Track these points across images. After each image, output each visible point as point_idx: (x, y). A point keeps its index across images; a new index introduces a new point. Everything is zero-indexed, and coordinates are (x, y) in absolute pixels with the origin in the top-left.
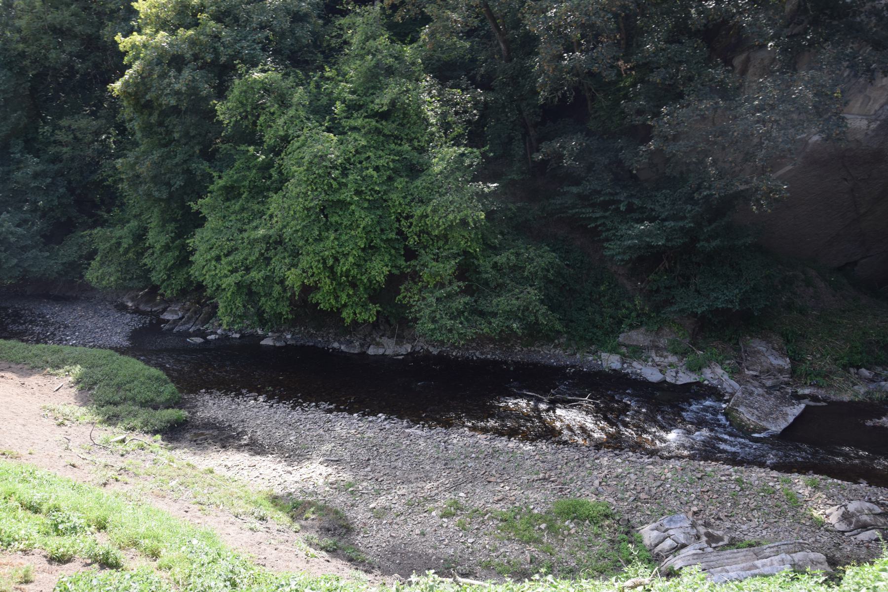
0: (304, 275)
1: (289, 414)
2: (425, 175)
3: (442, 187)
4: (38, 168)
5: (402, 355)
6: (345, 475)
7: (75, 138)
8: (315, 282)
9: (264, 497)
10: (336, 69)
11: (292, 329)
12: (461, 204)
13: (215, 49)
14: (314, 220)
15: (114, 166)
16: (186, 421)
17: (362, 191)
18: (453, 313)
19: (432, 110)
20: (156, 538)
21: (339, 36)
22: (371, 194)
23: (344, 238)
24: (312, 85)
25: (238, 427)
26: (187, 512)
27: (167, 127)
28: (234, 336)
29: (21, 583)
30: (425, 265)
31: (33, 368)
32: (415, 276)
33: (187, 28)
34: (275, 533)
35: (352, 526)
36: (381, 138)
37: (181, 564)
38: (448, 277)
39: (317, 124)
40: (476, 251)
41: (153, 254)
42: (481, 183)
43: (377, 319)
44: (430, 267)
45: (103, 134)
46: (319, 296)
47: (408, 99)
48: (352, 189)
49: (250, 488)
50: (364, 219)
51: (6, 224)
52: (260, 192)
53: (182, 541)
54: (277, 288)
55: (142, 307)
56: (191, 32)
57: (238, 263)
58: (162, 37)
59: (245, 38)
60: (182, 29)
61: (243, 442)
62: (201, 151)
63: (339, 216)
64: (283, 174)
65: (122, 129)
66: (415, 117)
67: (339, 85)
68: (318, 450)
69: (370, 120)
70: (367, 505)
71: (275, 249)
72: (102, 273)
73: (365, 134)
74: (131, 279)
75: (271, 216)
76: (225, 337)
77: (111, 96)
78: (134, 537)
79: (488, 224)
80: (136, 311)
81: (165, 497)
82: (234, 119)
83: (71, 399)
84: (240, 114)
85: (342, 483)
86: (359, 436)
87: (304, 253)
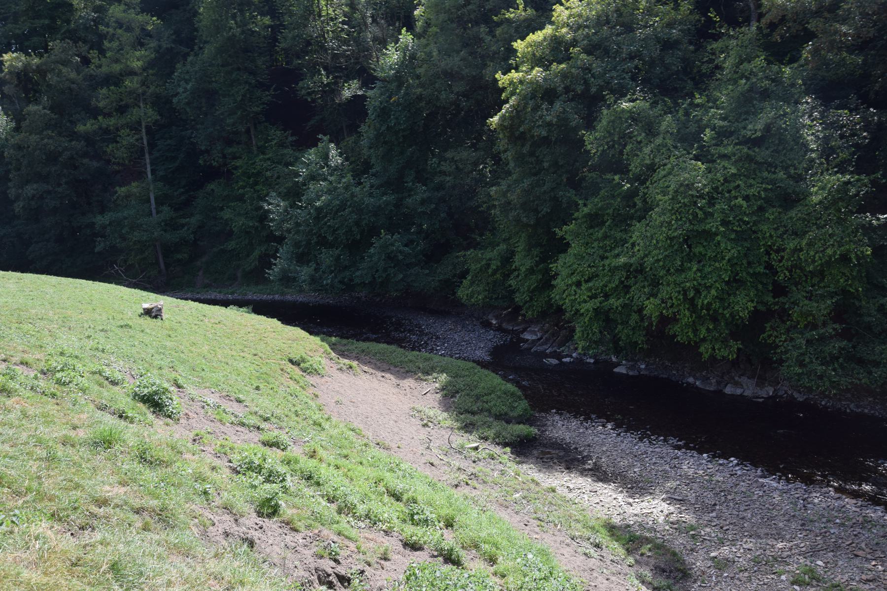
0: (663, 305)
1: (635, 445)
2: (801, 205)
3: (820, 218)
4: (425, 196)
5: (763, 398)
6: (687, 517)
7: (457, 168)
8: (674, 313)
9: (602, 524)
10: (707, 96)
11: (647, 360)
12: (842, 238)
13: (586, 82)
14: (676, 250)
15: (489, 194)
16: (535, 438)
17: (730, 221)
18: (825, 358)
19: (813, 134)
20: (496, 545)
21: (711, 61)
22: (739, 225)
23: (708, 269)
24: (681, 112)
25: (583, 451)
26: (526, 525)
27: (537, 157)
28: (588, 361)
29: (381, 559)
30: (795, 303)
31: (407, 372)
32: (784, 315)
33: (560, 63)
34: (609, 563)
35: (689, 572)
36: (753, 166)
37: (514, 575)
38: (822, 318)
39: (685, 152)
40: (857, 291)
41: (518, 276)
42: (868, 214)
43: (738, 357)
44: (801, 305)
45: (481, 164)
46: (677, 328)
47: (785, 123)
48: (719, 219)
49: (590, 513)
50: (729, 251)
51: (397, 244)
52: (623, 221)
53: (518, 553)
54: (635, 317)
55: (504, 325)
56: (563, 66)
57: (598, 289)
58: (537, 73)
59: (615, 68)
60: (555, 64)
61: (587, 467)
62: (568, 179)
63: (704, 247)
64: (647, 203)
65: (497, 159)
66: (792, 143)
67: (708, 112)
68: (662, 486)
69: (741, 147)
70: (707, 553)
71: (635, 277)
72: (472, 291)
73: (736, 162)
74: (496, 299)
75: (633, 245)
76: (579, 361)
77: (490, 130)
78: (476, 539)
79: (875, 261)
80: (499, 329)
81: (508, 507)
82: (601, 149)
83: (436, 403)
84: (607, 143)
85: (683, 525)
86: (707, 478)
87: (664, 283)
